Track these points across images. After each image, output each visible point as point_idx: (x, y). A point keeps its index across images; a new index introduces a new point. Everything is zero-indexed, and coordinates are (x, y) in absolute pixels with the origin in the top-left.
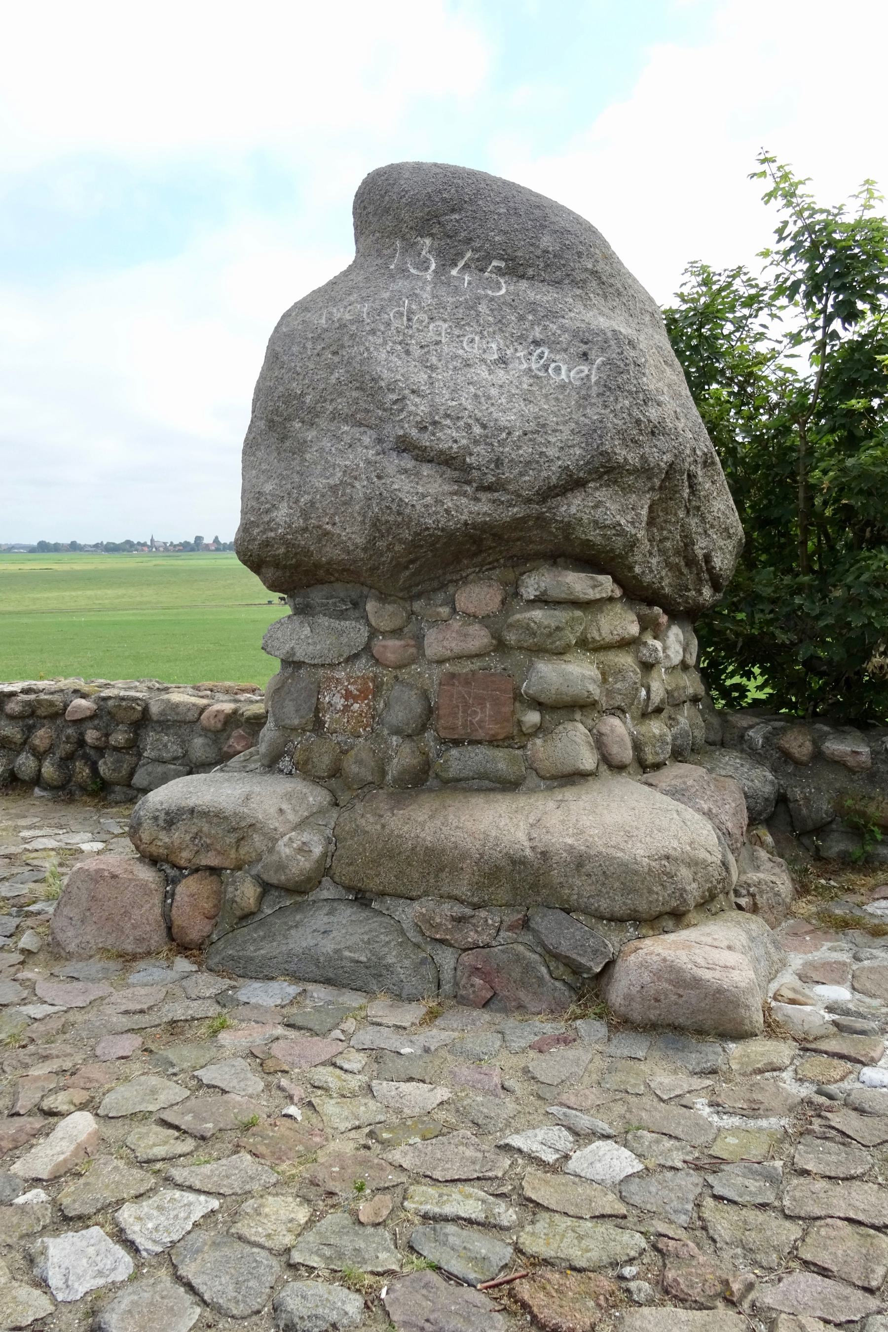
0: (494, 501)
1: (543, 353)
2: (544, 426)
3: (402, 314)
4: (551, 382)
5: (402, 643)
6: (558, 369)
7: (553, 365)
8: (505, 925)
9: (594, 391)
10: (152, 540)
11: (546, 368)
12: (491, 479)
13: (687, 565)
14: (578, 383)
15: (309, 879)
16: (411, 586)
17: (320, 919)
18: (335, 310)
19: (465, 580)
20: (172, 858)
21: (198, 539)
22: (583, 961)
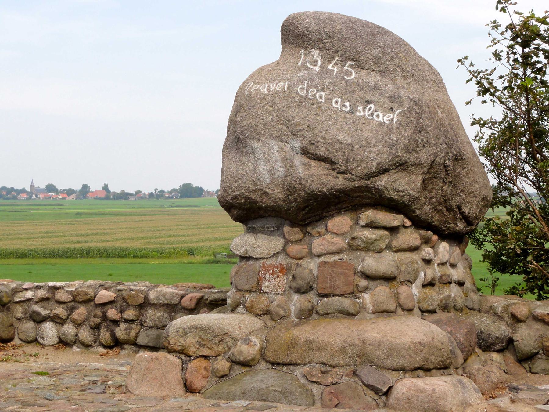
0: (345, 179)
1: (371, 107)
2: (369, 144)
3: (303, 89)
4: (374, 122)
5: (301, 247)
6: (378, 116)
7: (376, 114)
8: (345, 374)
9: (395, 126)
10: (32, 186)
11: (372, 115)
12: (344, 168)
13: (447, 210)
14: (387, 122)
15: (253, 359)
16: (305, 219)
17: (260, 377)
18: (271, 85)
19: (332, 216)
20: (185, 351)
21: (85, 187)
22: (379, 386)
